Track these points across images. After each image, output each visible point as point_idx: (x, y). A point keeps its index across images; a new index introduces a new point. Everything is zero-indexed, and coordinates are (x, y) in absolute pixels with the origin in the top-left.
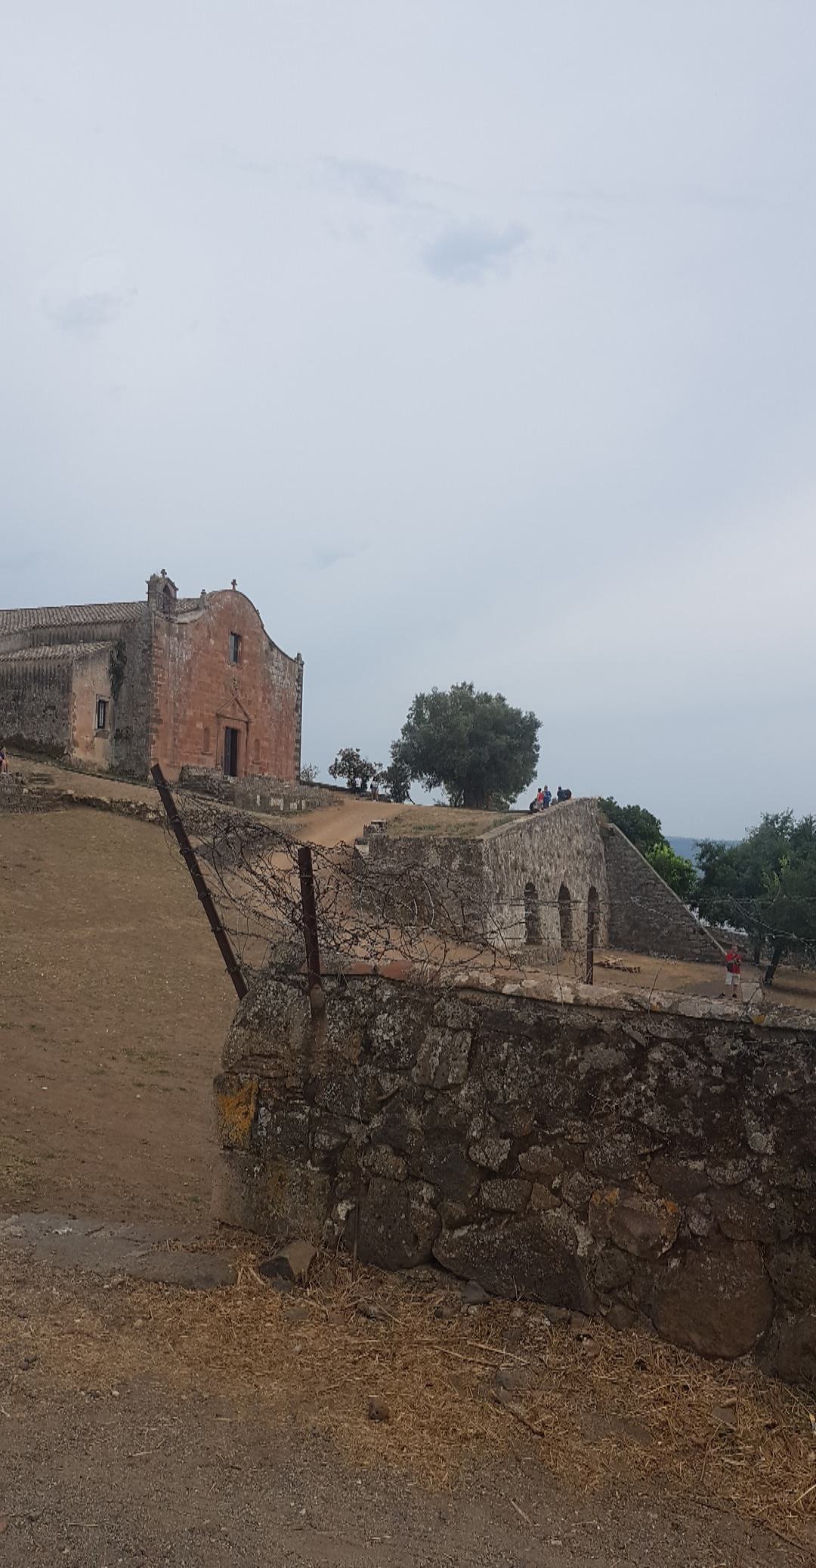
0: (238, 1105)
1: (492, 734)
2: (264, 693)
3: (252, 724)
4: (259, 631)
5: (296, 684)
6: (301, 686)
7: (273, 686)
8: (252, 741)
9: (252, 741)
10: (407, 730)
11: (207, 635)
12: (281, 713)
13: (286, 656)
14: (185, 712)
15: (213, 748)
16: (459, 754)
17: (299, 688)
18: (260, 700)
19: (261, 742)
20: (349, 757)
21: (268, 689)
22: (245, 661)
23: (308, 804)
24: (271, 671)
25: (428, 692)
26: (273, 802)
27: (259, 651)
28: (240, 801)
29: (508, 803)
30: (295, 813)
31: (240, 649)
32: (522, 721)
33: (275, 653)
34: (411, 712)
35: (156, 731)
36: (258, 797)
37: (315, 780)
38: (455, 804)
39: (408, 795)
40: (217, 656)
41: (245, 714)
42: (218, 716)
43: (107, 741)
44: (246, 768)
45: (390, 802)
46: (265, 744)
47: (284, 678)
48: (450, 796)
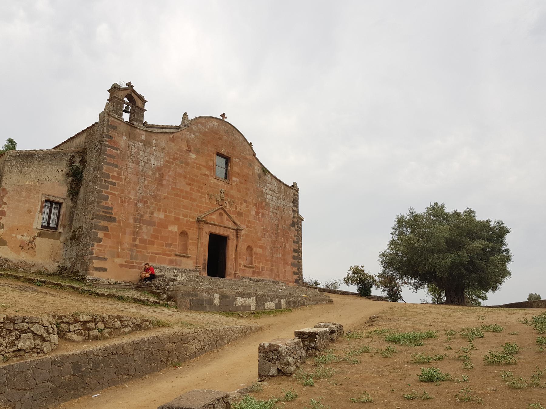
0: (392, 369)
1: (467, 240)
2: (258, 209)
3: (243, 232)
4: (251, 157)
5: (292, 205)
6: (297, 207)
7: (267, 204)
8: (243, 247)
9: (243, 247)
10: (393, 244)
11: (185, 148)
12: (277, 226)
13: (281, 182)
14: (152, 213)
15: (192, 250)
16: (439, 258)
17: (295, 209)
18: (253, 213)
19: (254, 249)
20: (357, 271)
21: (261, 205)
22: (234, 179)
23: (289, 303)
24: (264, 191)
25: (406, 214)
26: (239, 301)
27: (251, 173)
28: (186, 301)
29: (480, 300)
30: (271, 312)
31: (229, 168)
32: (492, 229)
33: (268, 177)
34: (394, 230)
35: (105, 229)
36: (217, 296)
37: (339, 289)
38: (438, 301)
39: (401, 297)
40: (200, 169)
41: (234, 223)
42: (199, 221)
43: (59, 243)
44: (236, 271)
45: (388, 301)
46: (260, 251)
47: (278, 199)
48: (432, 297)
